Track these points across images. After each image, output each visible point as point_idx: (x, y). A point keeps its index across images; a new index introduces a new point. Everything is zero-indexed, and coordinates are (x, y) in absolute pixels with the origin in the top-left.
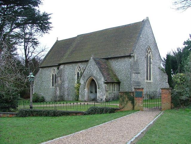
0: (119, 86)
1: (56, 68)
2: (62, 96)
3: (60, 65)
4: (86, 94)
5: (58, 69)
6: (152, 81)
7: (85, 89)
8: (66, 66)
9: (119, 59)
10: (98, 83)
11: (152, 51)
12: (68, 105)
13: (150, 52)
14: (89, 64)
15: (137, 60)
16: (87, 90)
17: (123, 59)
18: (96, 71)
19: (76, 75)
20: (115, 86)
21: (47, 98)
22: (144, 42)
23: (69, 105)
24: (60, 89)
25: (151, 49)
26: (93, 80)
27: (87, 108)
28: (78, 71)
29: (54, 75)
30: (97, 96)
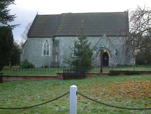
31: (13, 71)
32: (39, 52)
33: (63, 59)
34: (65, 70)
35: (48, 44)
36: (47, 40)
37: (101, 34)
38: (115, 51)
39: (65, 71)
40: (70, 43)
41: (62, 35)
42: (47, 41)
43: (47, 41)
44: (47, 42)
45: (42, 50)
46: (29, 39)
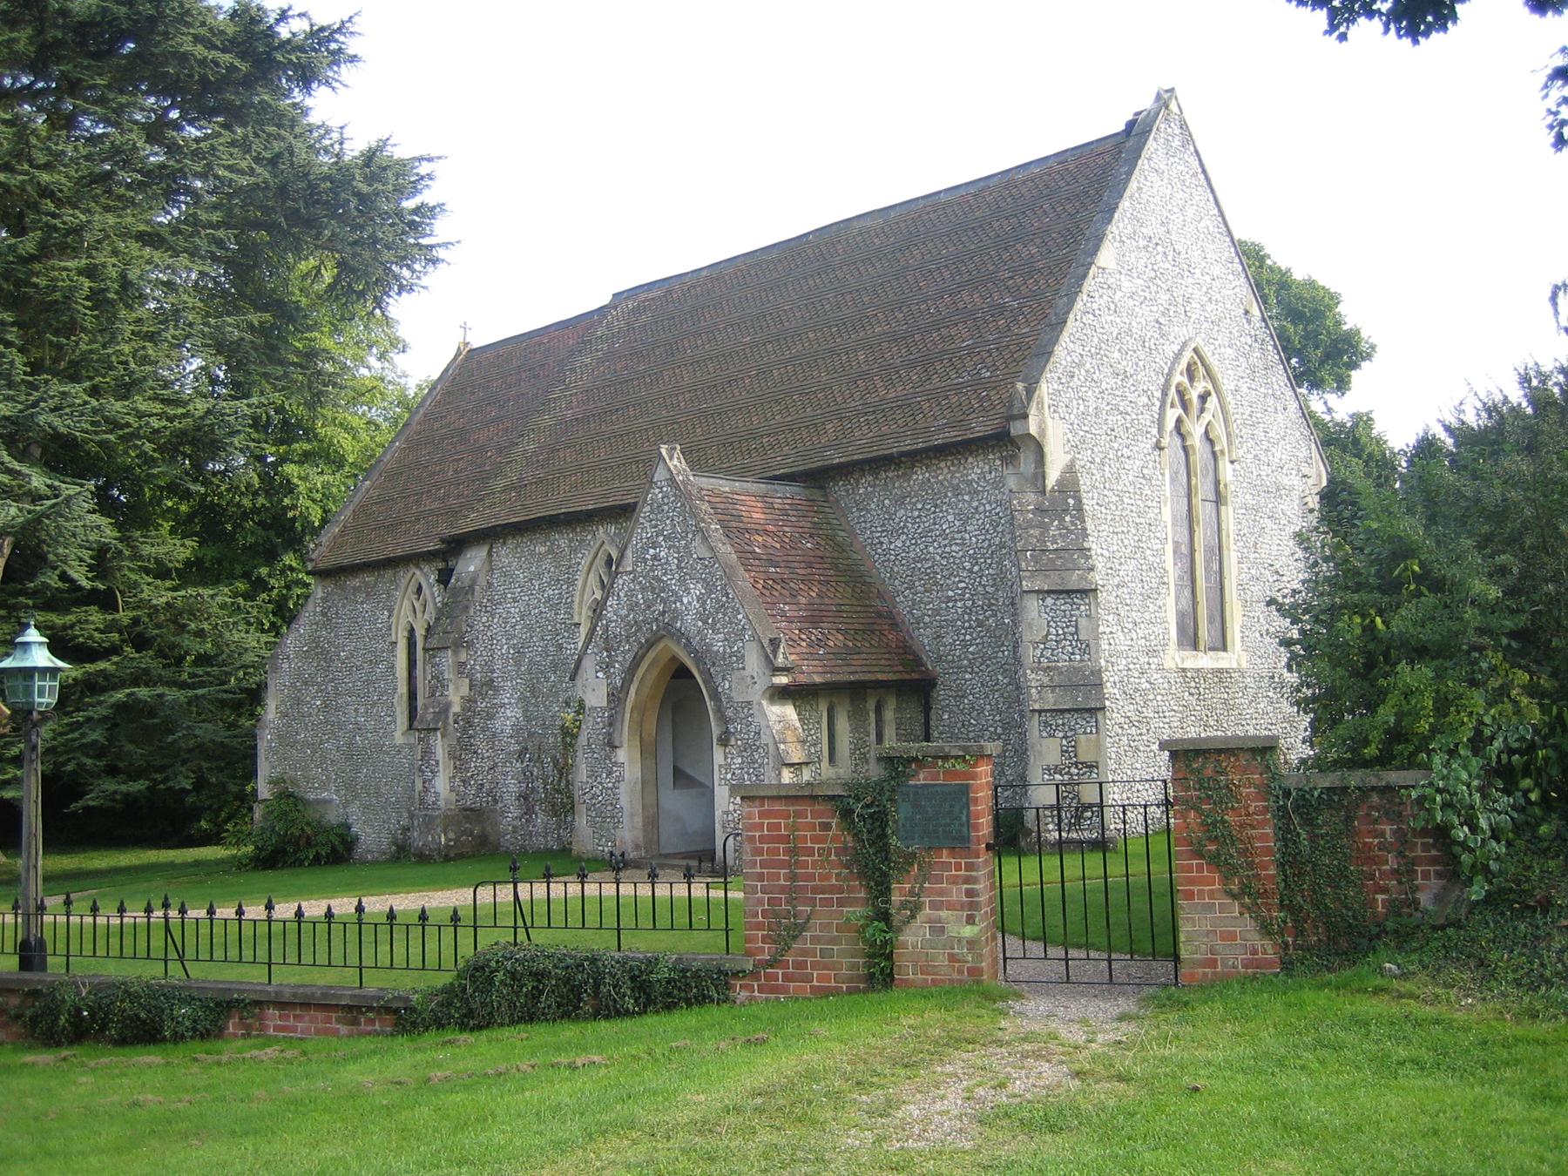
0: (927, 709)
1: (426, 576)
2: (472, 814)
3: (457, 545)
4: (628, 798)
5: (445, 577)
7: (621, 755)
8: (506, 554)
10: (715, 695)
11: (1227, 385)
13: (1204, 398)
14: (643, 530)
15: (1070, 469)
16: (631, 761)
17: (945, 473)
18: (697, 589)
20: (889, 714)
21: (371, 835)
22: (1145, 314)
24: (461, 753)
25: (1210, 374)
26: (681, 673)
27: (448, 963)
30: (718, 813)
46: (320, 595)
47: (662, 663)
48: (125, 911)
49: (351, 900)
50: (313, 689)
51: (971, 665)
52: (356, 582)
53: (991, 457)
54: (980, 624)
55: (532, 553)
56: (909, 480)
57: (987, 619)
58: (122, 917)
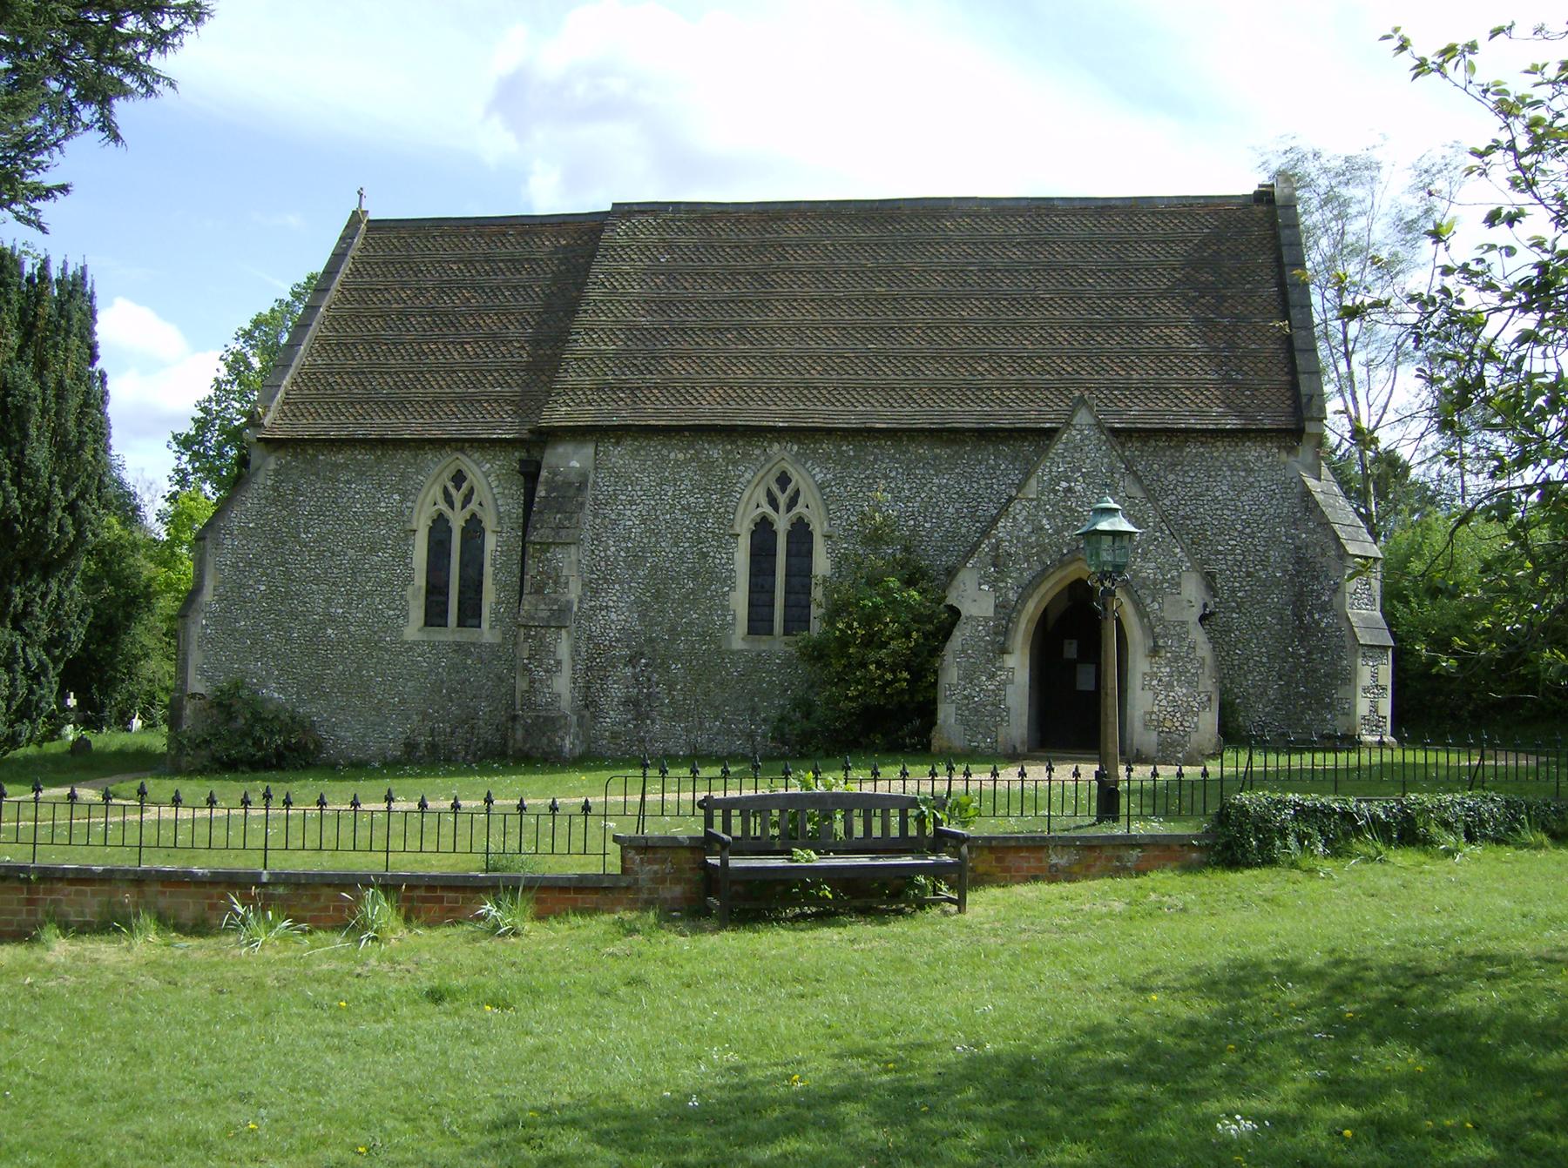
6: (487, 633)
8: (619, 455)
9: (1192, 449)
12: (974, 786)
14: (1045, 471)
19: (744, 544)
23: (988, 786)
28: (768, 509)
29: (782, 524)
31: (62, 812)
32: (371, 594)
33: (629, 671)
34: (727, 805)
35: (474, 515)
36: (459, 478)
37: (1030, 414)
38: (1192, 590)
39: (718, 812)
40: (709, 506)
41: (616, 421)
42: (458, 488)
43: (458, 488)
44: (458, 497)
45: (409, 580)
46: (272, 466)
47: (1067, 582)
48: (249, 803)
49: (1069, 766)
50: (258, 572)
51: (1238, 606)
52: (340, 458)
53: (1268, 444)
54: (1249, 574)
55: (664, 459)
56: (1181, 451)
57: (1257, 571)
58: (288, 809)
